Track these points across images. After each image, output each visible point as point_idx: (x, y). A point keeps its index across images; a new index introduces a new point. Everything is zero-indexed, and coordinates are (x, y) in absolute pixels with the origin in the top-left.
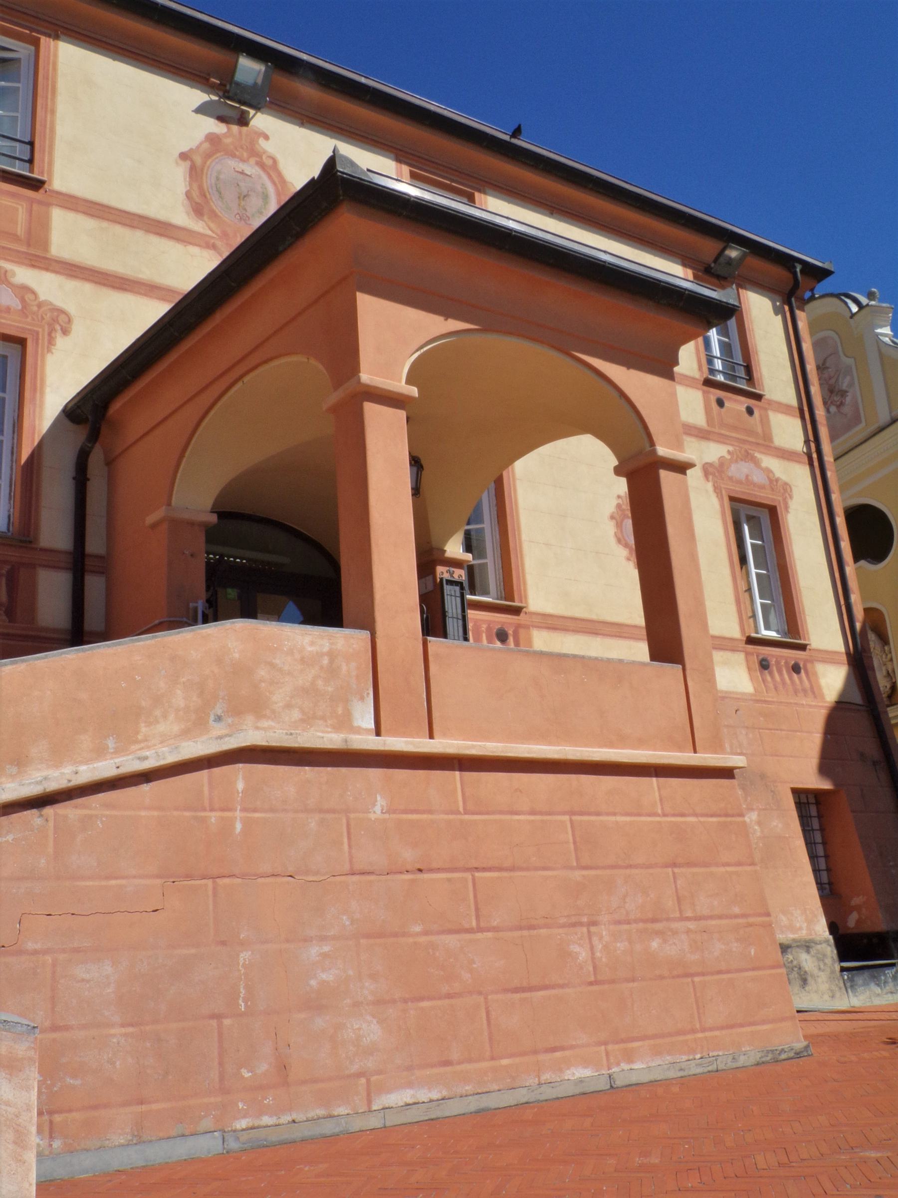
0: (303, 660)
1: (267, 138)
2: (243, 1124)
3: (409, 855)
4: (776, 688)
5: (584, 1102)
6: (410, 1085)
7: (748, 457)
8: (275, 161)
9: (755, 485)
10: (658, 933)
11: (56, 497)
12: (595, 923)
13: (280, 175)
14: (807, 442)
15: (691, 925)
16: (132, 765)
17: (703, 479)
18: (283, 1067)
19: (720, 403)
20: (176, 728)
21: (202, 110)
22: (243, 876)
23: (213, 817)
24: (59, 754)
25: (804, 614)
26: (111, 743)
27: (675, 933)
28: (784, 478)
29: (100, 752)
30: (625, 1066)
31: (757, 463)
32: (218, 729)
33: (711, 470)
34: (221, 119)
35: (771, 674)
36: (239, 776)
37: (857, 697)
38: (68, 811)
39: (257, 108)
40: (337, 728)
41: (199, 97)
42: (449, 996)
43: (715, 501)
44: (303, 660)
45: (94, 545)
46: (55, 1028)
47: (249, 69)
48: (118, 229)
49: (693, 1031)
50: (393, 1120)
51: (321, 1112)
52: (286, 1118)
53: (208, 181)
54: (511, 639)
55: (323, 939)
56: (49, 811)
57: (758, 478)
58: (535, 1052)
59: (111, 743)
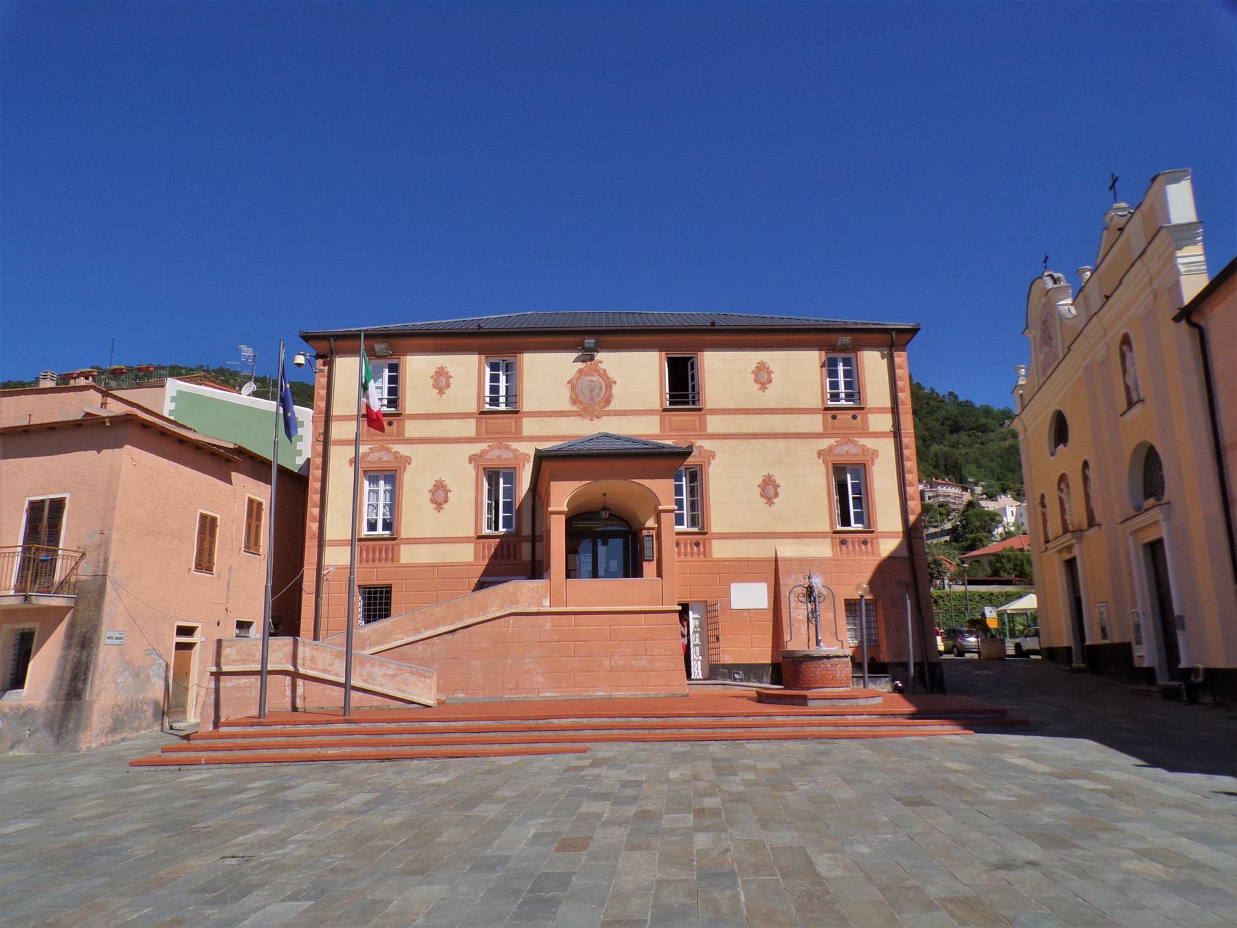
3: (556, 638)
5: (601, 699)
11: (527, 518)
19: (834, 417)
21: (576, 361)
24: (470, 616)
31: (855, 443)
36: (512, 619)
37: (905, 553)
41: (575, 355)
43: (823, 468)
45: (537, 533)
47: (589, 342)
48: (546, 419)
57: (854, 450)
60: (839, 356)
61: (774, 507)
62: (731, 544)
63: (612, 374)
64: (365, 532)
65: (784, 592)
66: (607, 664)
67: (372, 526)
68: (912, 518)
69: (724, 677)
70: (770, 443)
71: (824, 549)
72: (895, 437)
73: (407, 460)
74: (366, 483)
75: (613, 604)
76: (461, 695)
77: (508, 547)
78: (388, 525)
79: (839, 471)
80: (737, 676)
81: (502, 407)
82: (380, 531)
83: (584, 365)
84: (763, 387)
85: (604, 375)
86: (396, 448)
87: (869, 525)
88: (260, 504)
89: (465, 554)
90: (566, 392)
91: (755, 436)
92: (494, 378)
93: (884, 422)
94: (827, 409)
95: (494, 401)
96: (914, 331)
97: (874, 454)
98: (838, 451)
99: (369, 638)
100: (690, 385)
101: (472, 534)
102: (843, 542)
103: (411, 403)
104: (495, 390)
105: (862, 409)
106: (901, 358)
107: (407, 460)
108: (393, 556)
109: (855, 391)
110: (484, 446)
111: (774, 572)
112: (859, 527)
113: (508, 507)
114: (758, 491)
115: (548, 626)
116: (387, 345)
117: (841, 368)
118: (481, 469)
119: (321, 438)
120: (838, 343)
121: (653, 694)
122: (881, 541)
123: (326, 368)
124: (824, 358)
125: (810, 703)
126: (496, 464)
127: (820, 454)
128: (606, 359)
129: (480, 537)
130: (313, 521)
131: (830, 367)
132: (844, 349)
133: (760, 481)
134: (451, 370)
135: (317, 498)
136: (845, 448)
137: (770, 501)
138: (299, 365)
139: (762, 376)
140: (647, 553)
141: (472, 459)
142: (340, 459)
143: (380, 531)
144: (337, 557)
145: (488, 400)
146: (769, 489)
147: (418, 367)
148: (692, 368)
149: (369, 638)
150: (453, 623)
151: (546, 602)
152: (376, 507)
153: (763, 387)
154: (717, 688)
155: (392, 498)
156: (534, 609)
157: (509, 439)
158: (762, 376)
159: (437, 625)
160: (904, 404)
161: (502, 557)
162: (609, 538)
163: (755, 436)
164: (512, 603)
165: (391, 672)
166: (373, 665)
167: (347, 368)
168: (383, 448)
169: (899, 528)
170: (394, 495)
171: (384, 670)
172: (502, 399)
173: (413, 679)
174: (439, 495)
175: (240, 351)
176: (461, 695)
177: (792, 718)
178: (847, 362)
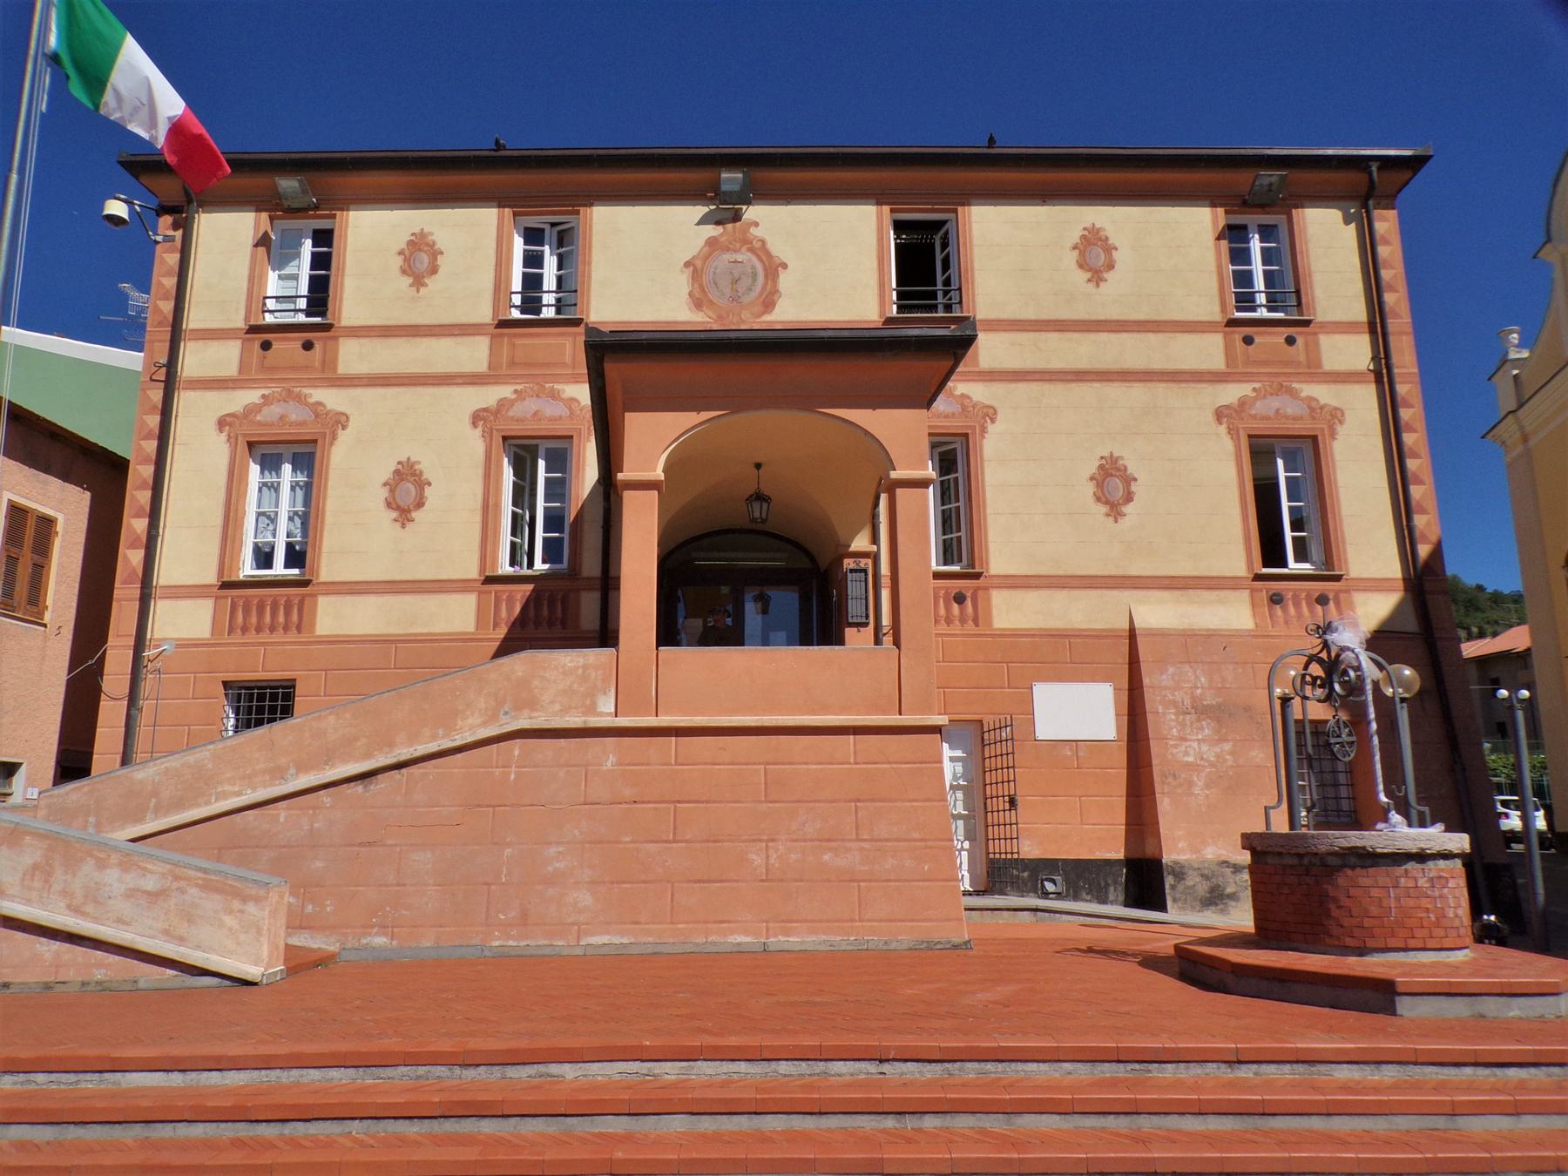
0: (564, 673)
1: (756, 224)
2: (497, 943)
3: (628, 792)
4: (1286, 622)
5: (741, 952)
6: (608, 933)
7: (1282, 390)
8: (763, 242)
9: (1287, 417)
10: (830, 849)
12: (773, 840)
13: (768, 254)
14: (1375, 358)
15: (866, 845)
16: (447, 744)
17: (1214, 424)
18: (524, 915)
19: (1248, 341)
20: (479, 721)
21: (703, 221)
22: (511, 806)
23: (497, 771)
24: (413, 739)
25: (1344, 542)
26: (441, 732)
27: (848, 850)
28: (1334, 403)
29: (434, 737)
30: (782, 938)
31: (1293, 394)
32: (504, 719)
33: (1226, 412)
34: (718, 223)
35: (1285, 610)
36: (516, 747)
37: (1411, 624)
38: (414, 770)
39: (749, 203)
40: (585, 714)
41: (701, 210)
42: (644, 882)
43: (1228, 444)
44: (564, 673)
46: (398, 885)
47: (731, 178)
49: (853, 920)
50: (590, 952)
51: (546, 942)
52: (523, 944)
53: (705, 279)
54: (969, 602)
55: (559, 843)
56: (404, 771)
57: (1291, 408)
58: (706, 922)
59: (441, 732)
60: (1251, 219)
61: (1125, 523)
62: (1032, 598)
63: (778, 248)
64: (247, 568)
65: (1153, 702)
66: (757, 860)
67: (264, 558)
68: (1424, 551)
69: (1021, 888)
70: (1114, 391)
71: (1234, 614)
72: (1379, 380)
73: (341, 420)
74: (254, 469)
75: (772, 709)
76: (380, 940)
77: (552, 603)
78: (295, 557)
79: (1261, 451)
80: (1050, 887)
81: (548, 313)
82: (279, 569)
83: (720, 229)
84: (1097, 277)
85: (761, 250)
86: (318, 395)
87: (1328, 561)
88: (47, 523)
89: (458, 615)
90: (681, 284)
91: (1080, 376)
92: (533, 260)
93: (1356, 352)
94: (1233, 323)
95: (531, 303)
96: (1415, 164)
97: (1336, 416)
98: (1260, 407)
99: (155, 793)
100: (940, 279)
101: (472, 572)
102: (1276, 599)
103: (351, 306)
104: (532, 283)
105: (1307, 323)
106: (1386, 223)
107: (341, 420)
108: (300, 619)
109: (1289, 290)
110: (506, 391)
111: (1131, 664)
112: (1305, 568)
113: (553, 521)
114: (1090, 488)
115: (610, 761)
116: (302, 184)
117: (1256, 245)
118: (498, 441)
119: (162, 374)
120: (1254, 192)
121: (875, 940)
122: (1359, 598)
123: (179, 234)
124: (1222, 223)
125: (1404, 1006)
126: (531, 428)
127: (1220, 414)
128: (765, 218)
129: (491, 580)
130: (133, 546)
131: (1234, 235)
132: (1263, 206)
133: (1092, 467)
134: (441, 238)
135: (144, 497)
136: (1274, 403)
137: (1115, 510)
138: (114, 220)
139: (1095, 255)
140: (854, 609)
141: (477, 418)
142: (197, 416)
143: (279, 569)
144: (180, 622)
145: (517, 300)
146: (1113, 486)
147: (371, 233)
148: (945, 245)
149: (155, 793)
150: (368, 756)
151: (607, 704)
152: (273, 519)
153: (1097, 277)
154: (1017, 919)
155: (307, 502)
156: (574, 721)
157: (557, 378)
158: (1095, 255)
159: (329, 758)
160: (1397, 316)
161: (538, 624)
162: (759, 573)
163: (1080, 376)
164: (518, 707)
165: (150, 884)
166: (101, 865)
167: (225, 237)
168: (290, 396)
169: (1393, 569)
170: (310, 492)
171: (131, 879)
172: (549, 299)
173: (211, 903)
174: (406, 492)
175: (126, 297)
176: (380, 940)
177: (1390, 1073)
178: (1267, 232)
